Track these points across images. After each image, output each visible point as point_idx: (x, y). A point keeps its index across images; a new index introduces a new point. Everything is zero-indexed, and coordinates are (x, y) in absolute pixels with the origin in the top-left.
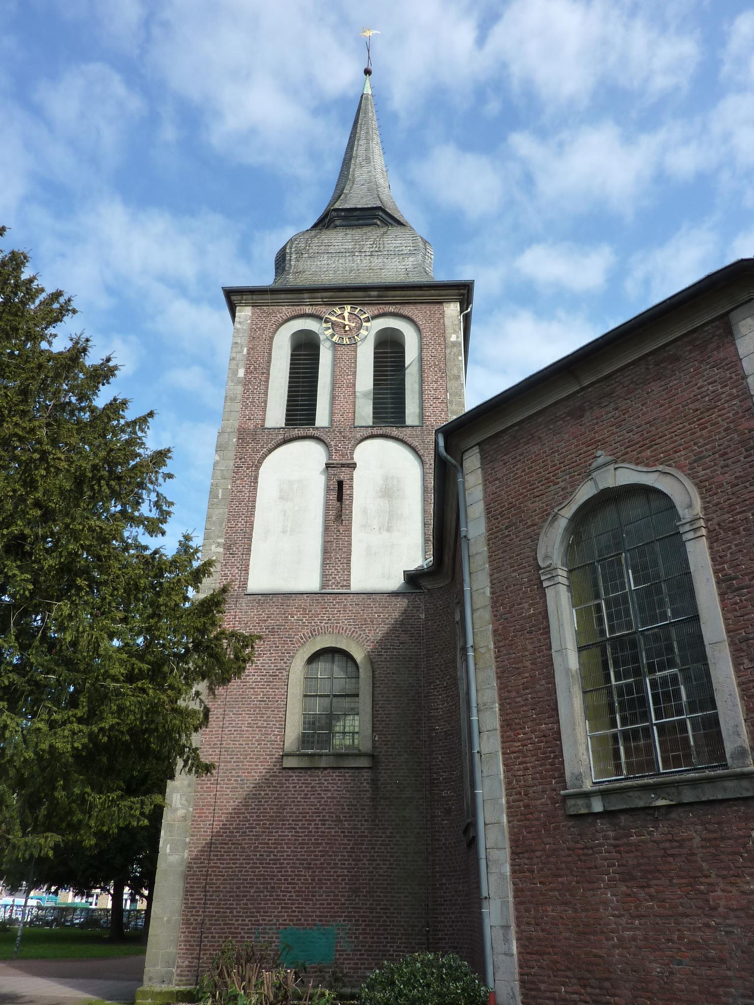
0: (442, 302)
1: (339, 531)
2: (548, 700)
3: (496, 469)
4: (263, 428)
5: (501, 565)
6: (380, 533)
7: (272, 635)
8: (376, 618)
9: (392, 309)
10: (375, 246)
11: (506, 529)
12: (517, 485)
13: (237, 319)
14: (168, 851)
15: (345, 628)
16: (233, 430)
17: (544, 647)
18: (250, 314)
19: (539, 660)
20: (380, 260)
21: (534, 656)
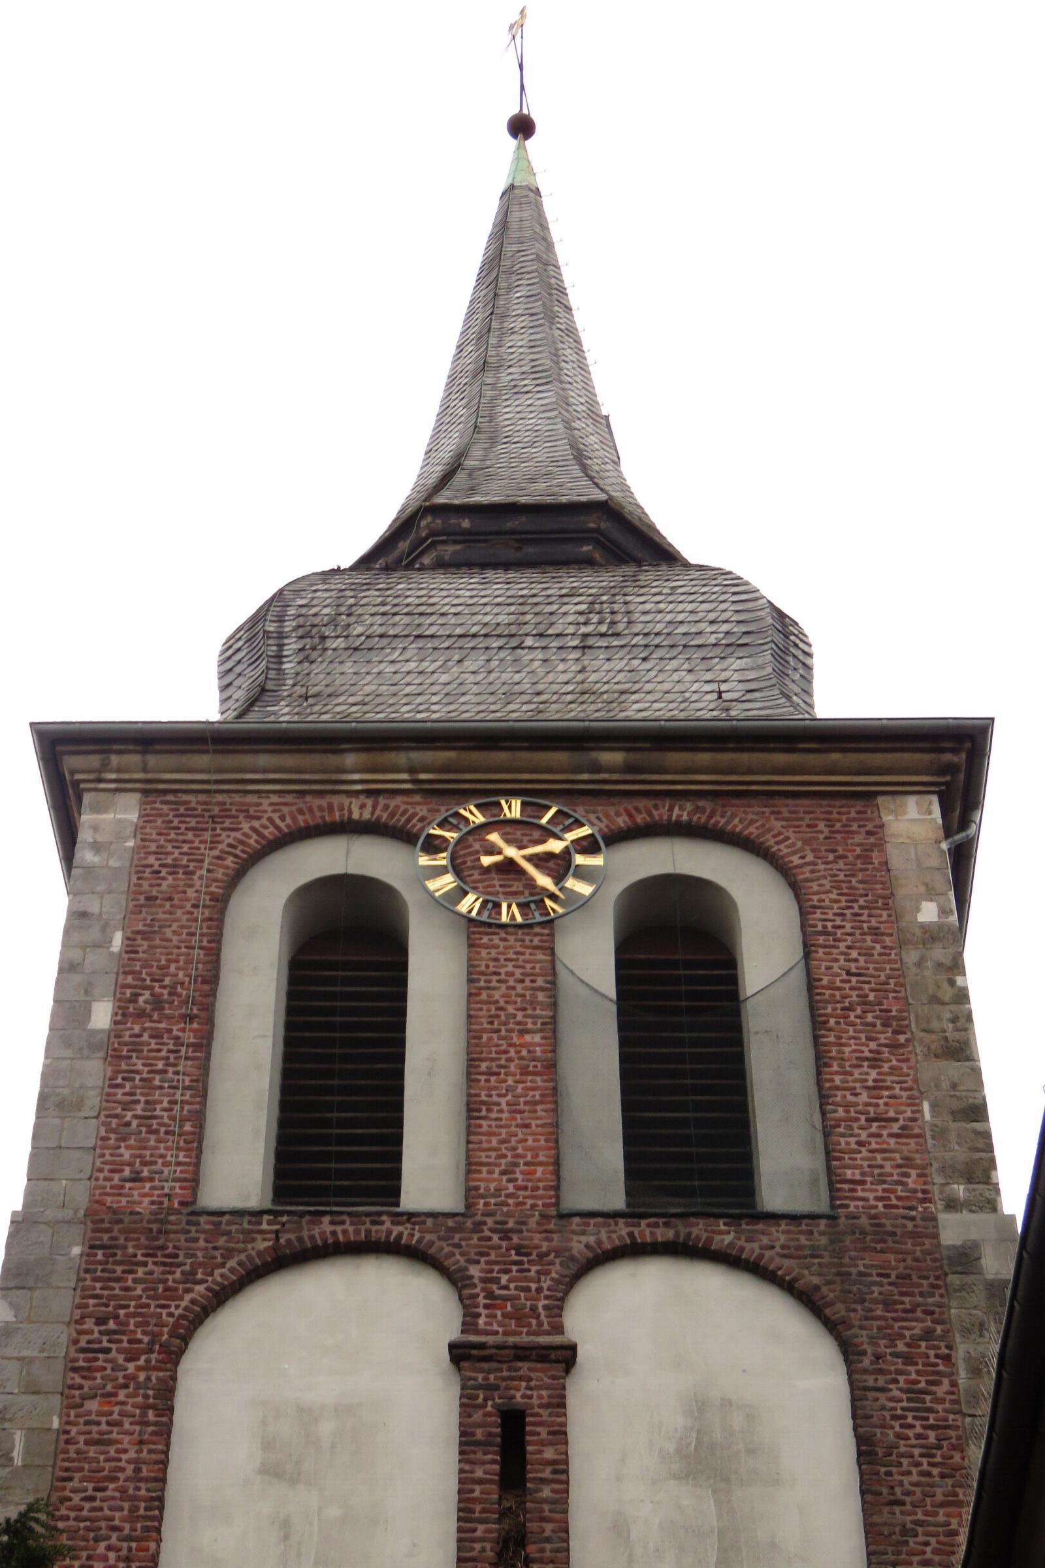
4: (192, 1211)
9: (682, 813)
10: (595, 618)
16: (68, 1214)
18: (133, 817)
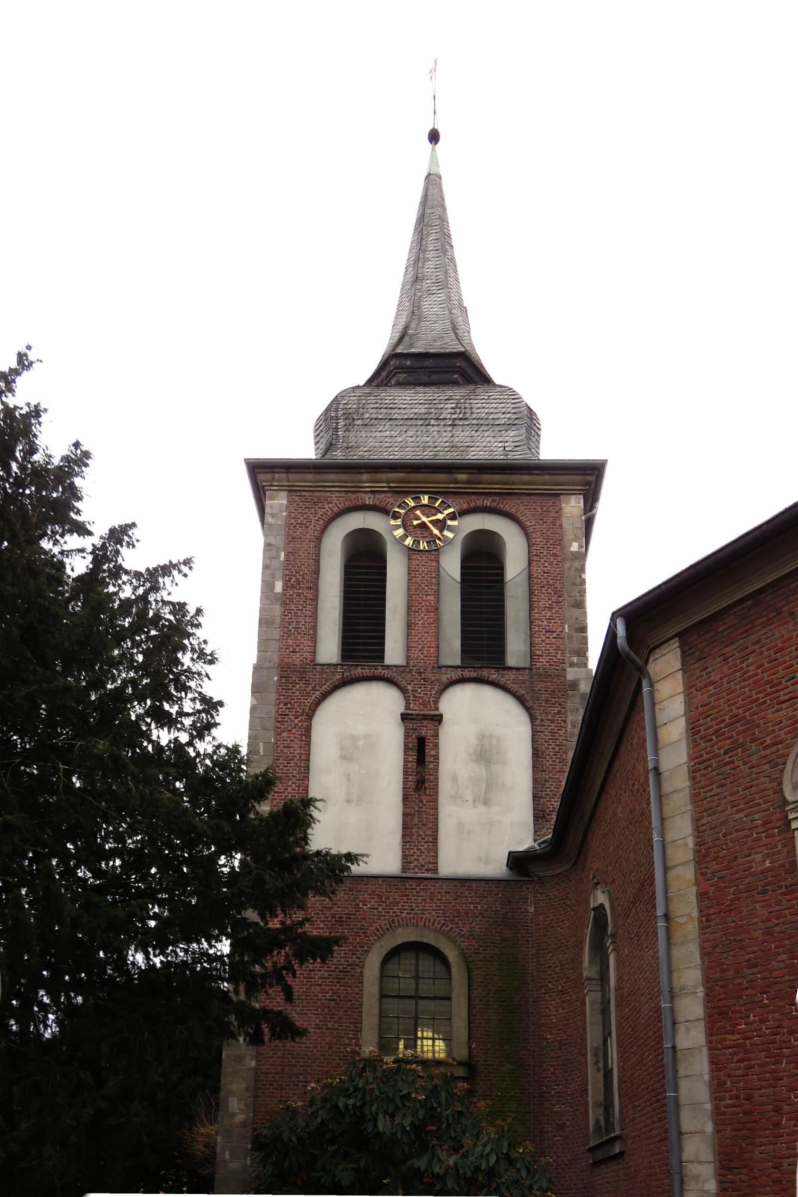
0: (559, 495)
1: (421, 801)
2: (790, 981)
3: (709, 669)
5: (715, 804)
6: (475, 807)
7: (339, 925)
8: (471, 910)
11: (726, 753)
12: (747, 689)
13: (268, 510)
14: (227, 1156)
15: (432, 921)
17: (786, 911)
18: (285, 502)
19: (778, 929)
20: (467, 433)
21: (769, 924)
